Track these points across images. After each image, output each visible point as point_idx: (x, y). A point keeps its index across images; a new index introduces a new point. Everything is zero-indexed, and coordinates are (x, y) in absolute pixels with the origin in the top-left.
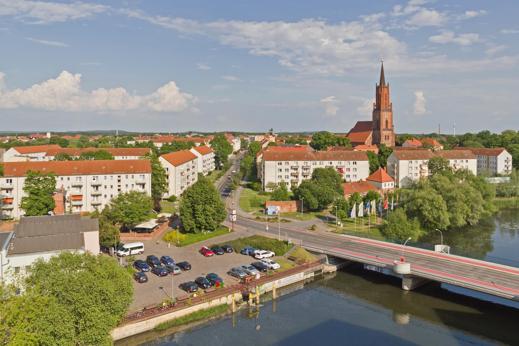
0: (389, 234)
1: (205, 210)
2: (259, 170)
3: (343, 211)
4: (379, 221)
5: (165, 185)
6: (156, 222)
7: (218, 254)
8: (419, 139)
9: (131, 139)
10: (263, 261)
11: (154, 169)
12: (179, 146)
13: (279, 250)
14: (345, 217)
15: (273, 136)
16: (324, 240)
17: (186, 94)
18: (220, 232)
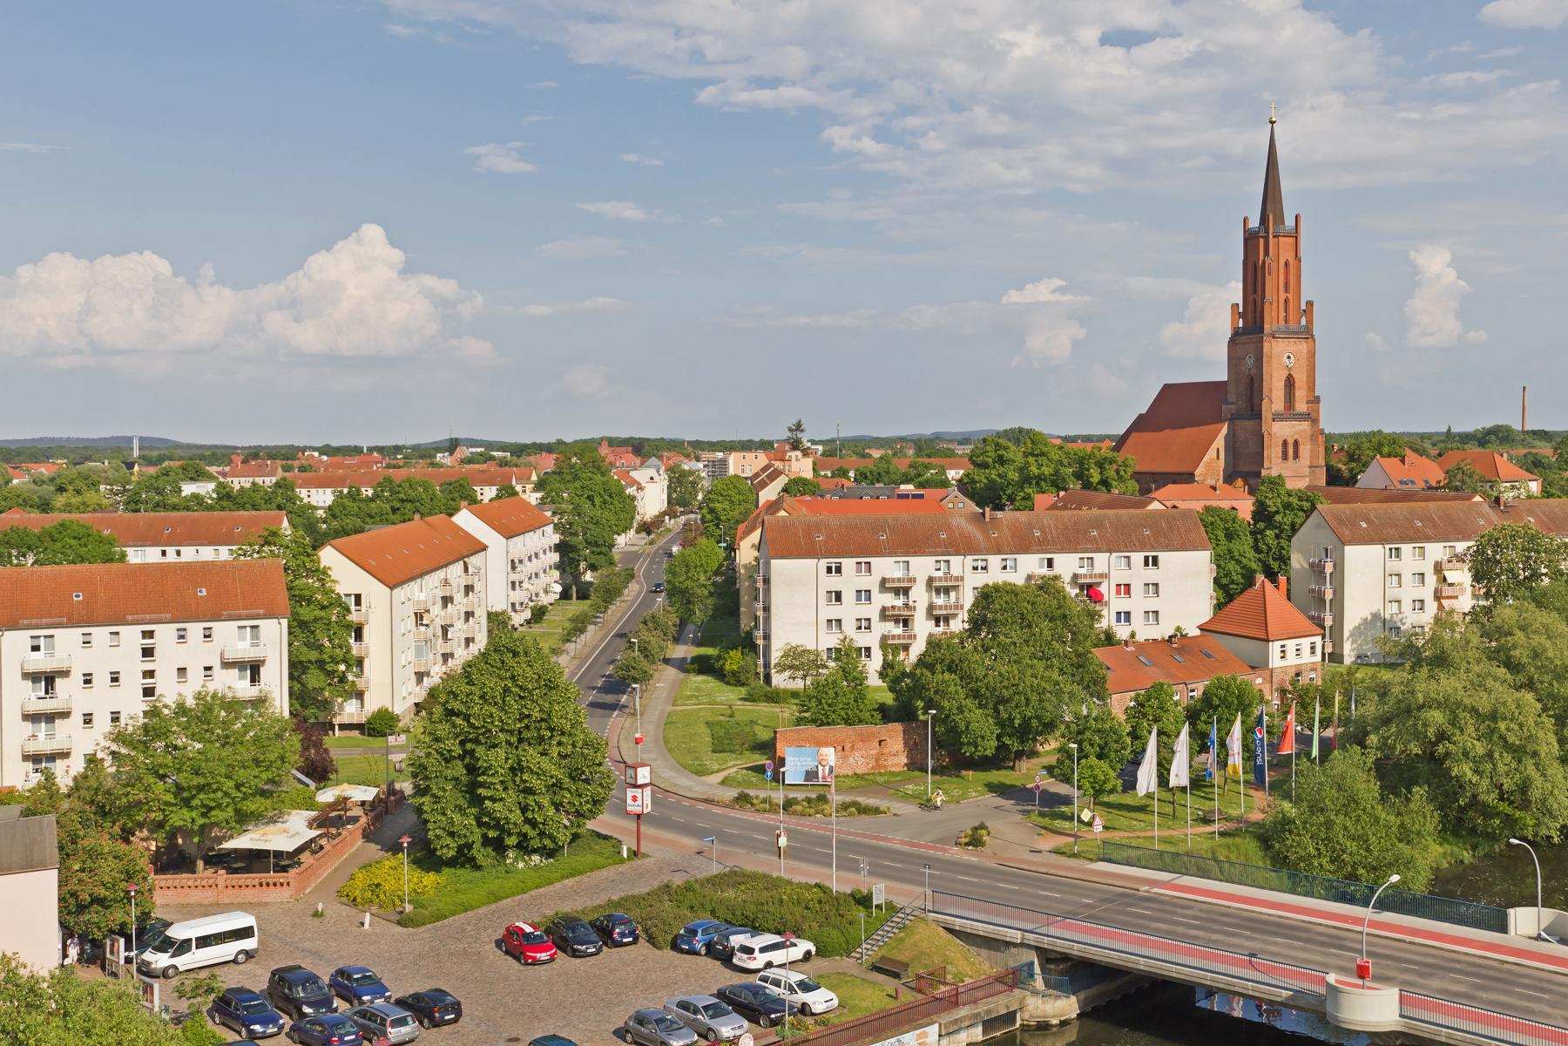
0: (1301, 859)
1: (522, 769)
2: (744, 598)
4: (1257, 806)
5: (349, 666)
6: (310, 826)
7: (575, 954)
9: (198, 476)
10: (765, 979)
11: (302, 598)
12: (404, 503)
13: (835, 933)
14: (1112, 791)
15: (806, 453)
16: (1020, 889)
17: (430, 281)
18: (585, 859)
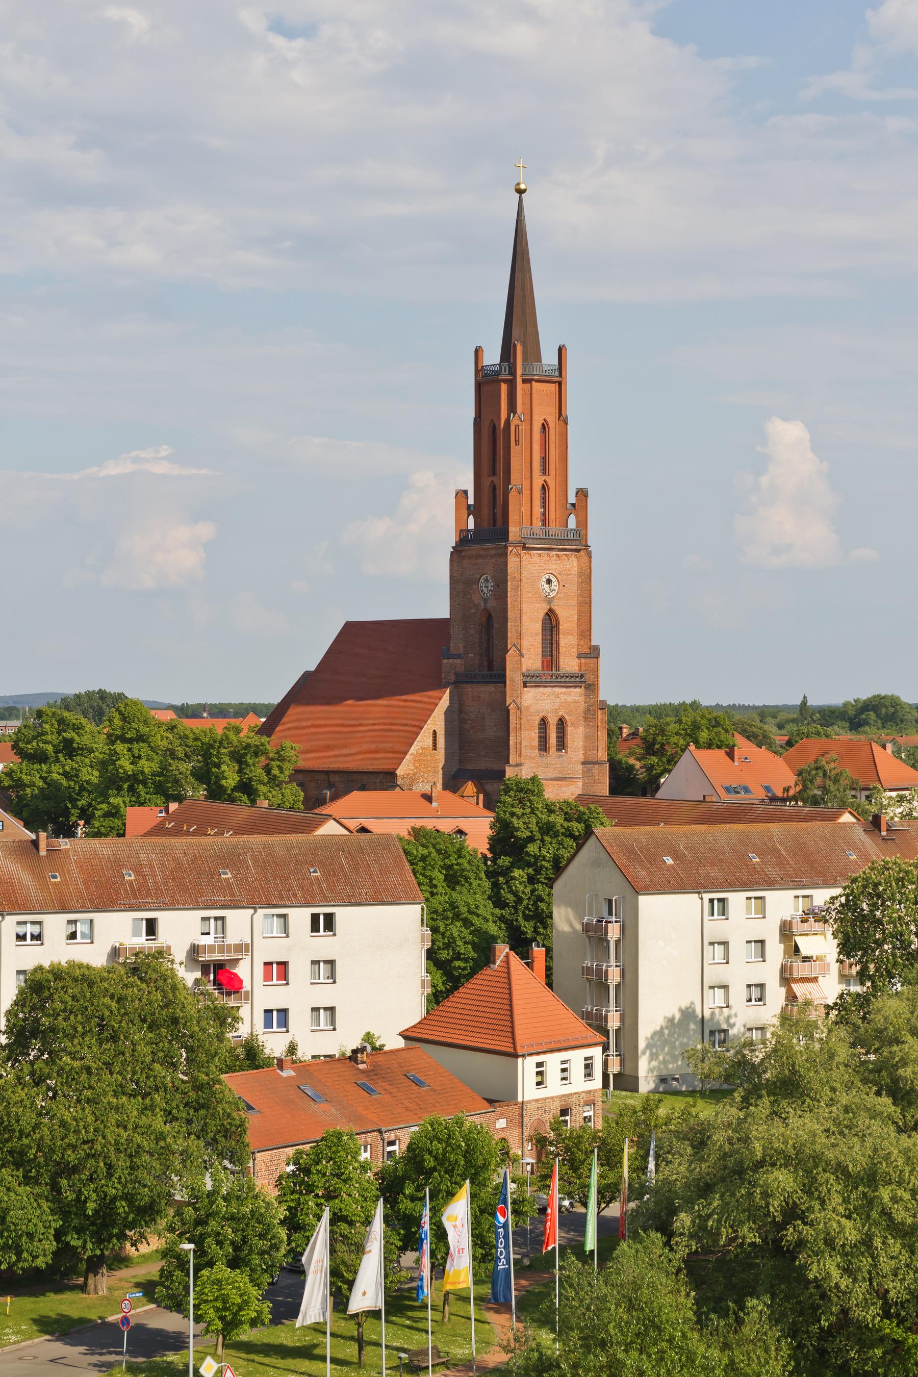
3: (240, 1278)
8: (779, 738)
